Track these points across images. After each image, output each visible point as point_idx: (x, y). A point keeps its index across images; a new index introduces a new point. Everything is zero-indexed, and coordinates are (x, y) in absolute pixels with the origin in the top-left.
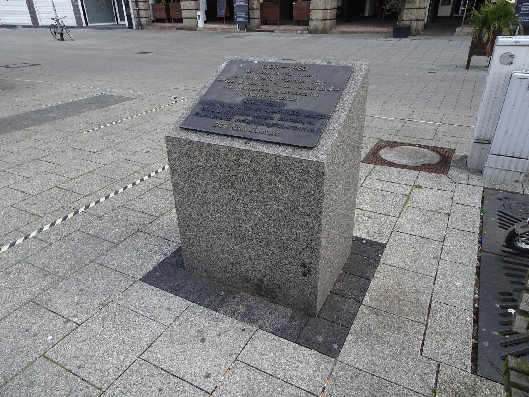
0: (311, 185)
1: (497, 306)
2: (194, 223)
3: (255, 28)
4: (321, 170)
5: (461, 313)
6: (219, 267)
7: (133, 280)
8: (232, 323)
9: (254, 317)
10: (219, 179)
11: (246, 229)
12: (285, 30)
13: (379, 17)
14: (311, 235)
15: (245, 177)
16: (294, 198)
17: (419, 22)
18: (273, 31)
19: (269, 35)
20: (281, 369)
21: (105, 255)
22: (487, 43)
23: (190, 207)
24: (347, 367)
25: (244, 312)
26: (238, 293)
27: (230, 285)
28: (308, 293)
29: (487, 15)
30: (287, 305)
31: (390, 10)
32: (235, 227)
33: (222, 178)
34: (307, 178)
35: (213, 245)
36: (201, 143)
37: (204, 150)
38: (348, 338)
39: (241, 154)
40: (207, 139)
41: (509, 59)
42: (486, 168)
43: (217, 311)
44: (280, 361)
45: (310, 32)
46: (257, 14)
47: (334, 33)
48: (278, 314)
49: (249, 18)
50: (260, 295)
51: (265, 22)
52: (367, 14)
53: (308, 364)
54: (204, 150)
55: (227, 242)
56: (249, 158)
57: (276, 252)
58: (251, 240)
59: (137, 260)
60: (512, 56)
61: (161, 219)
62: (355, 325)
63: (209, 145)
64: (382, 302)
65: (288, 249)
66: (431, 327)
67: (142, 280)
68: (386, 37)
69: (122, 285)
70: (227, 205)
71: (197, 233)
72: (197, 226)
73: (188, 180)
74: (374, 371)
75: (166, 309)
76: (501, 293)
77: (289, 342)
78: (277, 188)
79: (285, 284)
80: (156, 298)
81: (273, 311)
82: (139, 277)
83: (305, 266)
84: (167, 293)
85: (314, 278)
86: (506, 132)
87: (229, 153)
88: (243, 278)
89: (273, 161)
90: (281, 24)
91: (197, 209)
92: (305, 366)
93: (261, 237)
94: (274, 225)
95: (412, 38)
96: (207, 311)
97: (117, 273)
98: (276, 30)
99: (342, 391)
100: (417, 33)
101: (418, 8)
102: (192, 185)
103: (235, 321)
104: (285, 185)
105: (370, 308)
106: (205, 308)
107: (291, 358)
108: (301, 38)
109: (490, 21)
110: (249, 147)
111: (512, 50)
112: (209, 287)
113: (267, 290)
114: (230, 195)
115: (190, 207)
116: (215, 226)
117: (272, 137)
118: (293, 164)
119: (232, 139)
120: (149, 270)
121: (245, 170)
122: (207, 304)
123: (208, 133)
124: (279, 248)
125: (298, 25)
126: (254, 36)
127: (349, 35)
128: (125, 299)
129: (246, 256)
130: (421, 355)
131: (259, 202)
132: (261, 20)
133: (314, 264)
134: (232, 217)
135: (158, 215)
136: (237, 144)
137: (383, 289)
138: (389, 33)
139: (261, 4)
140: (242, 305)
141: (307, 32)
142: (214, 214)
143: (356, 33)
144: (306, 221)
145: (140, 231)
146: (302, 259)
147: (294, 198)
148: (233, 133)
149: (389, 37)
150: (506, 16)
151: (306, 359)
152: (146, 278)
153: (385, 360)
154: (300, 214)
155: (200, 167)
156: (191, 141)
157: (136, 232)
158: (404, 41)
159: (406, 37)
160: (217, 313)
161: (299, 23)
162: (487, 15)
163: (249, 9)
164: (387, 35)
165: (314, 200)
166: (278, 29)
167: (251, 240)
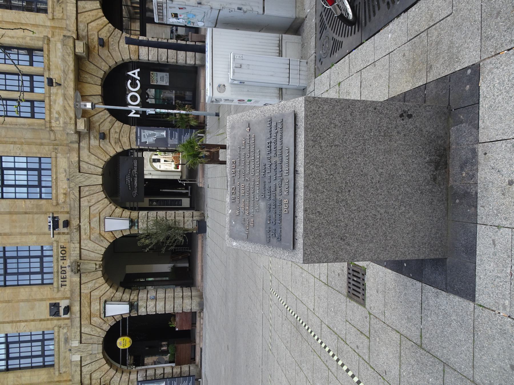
0: (325, 109)
1: (398, 3)
2: (388, 238)
3: (198, 369)
4: (312, 99)
5: (411, 17)
6: (430, 211)
7: (478, 310)
8: (483, 170)
9: (470, 155)
10: (337, 202)
11: (380, 175)
12: (200, 336)
13: (189, 255)
14: (370, 109)
15: (329, 173)
16: (339, 124)
17: (194, 215)
18: (201, 349)
19: (205, 352)
20: (507, 95)
21: (460, 369)
22: (210, 151)
23: (372, 242)
24: (483, 49)
25: (469, 166)
26: (452, 187)
27: (447, 200)
28: (428, 113)
29: (190, 155)
30: (448, 135)
31: (184, 238)
32: (381, 187)
33: (335, 198)
34: (320, 112)
35: (407, 216)
36: (304, 219)
37: (311, 216)
38: (458, 69)
39: (309, 176)
40: (300, 215)
41: (222, 87)
42: (301, 85)
43: (476, 193)
44: (501, 100)
45: (202, 310)
46: (185, 368)
47: (203, 286)
48: (458, 137)
49: (189, 376)
50: (446, 164)
51: (192, 360)
52: (187, 265)
53: (494, 78)
54: (311, 216)
55: (400, 198)
56: (311, 167)
57: (396, 145)
58: (391, 172)
59: (454, 324)
60: (219, 86)
61: (401, 331)
62: (447, 73)
63: (305, 210)
64: (420, 71)
65: (389, 131)
66: (429, 25)
67: (474, 300)
68: (206, 238)
69: (487, 319)
70: (361, 196)
71: (399, 235)
72: (390, 235)
73: (344, 240)
74: (478, 30)
75: (495, 246)
76: (389, 8)
77: (480, 107)
78: (334, 140)
79: (426, 136)
80: (487, 267)
81: (457, 144)
82: (472, 304)
83: (401, 116)
84: (478, 258)
85: (411, 107)
86: (272, 76)
87: (310, 188)
88: (434, 183)
89: (311, 143)
90: (195, 342)
91: (372, 233)
92: (496, 79)
93: (384, 160)
94: (369, 145)
95: (206, 218)
96: (480, 202)
97: (476, 337)
98: (200, 346)
99: (504, 36)
100: (203, 215)
101: (184, 218)
102: (348, 235)
103: (480, 168)
104: (330, 133)
105: (428, 75)
106: (479, 207)
107: (494, 95)
108: (207, 317)
109: (195, 153)
110: (301, 169)
111: (215, 86)
112: (456, 220)
113: (439, 156)
114: (349, 191)
115: (372, 242)
116: (385, 212)
117: (291, 151)
118: (310, 124)
119: (297, 190)
120: (461, 300)
121: (323, 173)
122: (473, 208)
123: (295, 216)
124: (390, 141)
125: (195, 324)
126: (206, 369)
127: (204, 272)
128: (501, 302)
129: (408, 178)
130: (452, 13)
131: (350, 160)
132: (191, 363)
133: (397, 106)
134: (371, 190)
135: (398, 336)
136: (301, 182)
137: (409, 79)
138: (203, 238)
139: (176, 365)
140: (462, 174)
141: (202, 313)
142: (374, 212)
143: (202, 266)
144: (358, 114)
145: (421, 346)
146: (395, 118)
147: (339, 124)
148: (291, 190)
149: (205, 236)
150: (191, 143)
151: (490, 83)
152: (470, 295)
153: (465, 31)
154: (353, 119)
155: (329, 223)
156: (304, 231)
157: (423, 349)
158: (209, 223)
159: (205, 222)
160: (479, 191)
161: (194, 324)
162: (190, 155)
163: (181, 377)
164: (204, 239)
165: (338, 105)
166: (199, 344)
167: (391, 172)
